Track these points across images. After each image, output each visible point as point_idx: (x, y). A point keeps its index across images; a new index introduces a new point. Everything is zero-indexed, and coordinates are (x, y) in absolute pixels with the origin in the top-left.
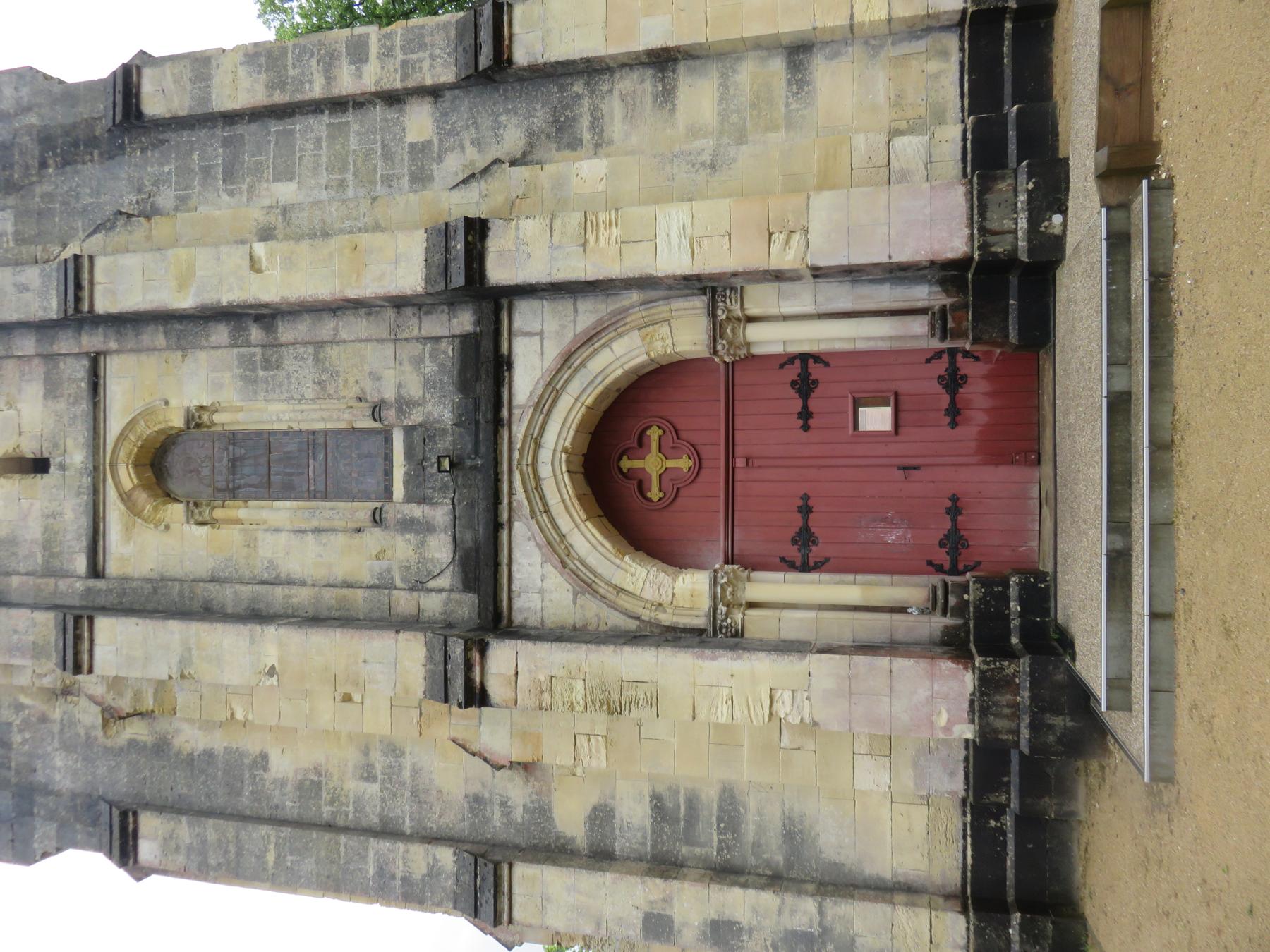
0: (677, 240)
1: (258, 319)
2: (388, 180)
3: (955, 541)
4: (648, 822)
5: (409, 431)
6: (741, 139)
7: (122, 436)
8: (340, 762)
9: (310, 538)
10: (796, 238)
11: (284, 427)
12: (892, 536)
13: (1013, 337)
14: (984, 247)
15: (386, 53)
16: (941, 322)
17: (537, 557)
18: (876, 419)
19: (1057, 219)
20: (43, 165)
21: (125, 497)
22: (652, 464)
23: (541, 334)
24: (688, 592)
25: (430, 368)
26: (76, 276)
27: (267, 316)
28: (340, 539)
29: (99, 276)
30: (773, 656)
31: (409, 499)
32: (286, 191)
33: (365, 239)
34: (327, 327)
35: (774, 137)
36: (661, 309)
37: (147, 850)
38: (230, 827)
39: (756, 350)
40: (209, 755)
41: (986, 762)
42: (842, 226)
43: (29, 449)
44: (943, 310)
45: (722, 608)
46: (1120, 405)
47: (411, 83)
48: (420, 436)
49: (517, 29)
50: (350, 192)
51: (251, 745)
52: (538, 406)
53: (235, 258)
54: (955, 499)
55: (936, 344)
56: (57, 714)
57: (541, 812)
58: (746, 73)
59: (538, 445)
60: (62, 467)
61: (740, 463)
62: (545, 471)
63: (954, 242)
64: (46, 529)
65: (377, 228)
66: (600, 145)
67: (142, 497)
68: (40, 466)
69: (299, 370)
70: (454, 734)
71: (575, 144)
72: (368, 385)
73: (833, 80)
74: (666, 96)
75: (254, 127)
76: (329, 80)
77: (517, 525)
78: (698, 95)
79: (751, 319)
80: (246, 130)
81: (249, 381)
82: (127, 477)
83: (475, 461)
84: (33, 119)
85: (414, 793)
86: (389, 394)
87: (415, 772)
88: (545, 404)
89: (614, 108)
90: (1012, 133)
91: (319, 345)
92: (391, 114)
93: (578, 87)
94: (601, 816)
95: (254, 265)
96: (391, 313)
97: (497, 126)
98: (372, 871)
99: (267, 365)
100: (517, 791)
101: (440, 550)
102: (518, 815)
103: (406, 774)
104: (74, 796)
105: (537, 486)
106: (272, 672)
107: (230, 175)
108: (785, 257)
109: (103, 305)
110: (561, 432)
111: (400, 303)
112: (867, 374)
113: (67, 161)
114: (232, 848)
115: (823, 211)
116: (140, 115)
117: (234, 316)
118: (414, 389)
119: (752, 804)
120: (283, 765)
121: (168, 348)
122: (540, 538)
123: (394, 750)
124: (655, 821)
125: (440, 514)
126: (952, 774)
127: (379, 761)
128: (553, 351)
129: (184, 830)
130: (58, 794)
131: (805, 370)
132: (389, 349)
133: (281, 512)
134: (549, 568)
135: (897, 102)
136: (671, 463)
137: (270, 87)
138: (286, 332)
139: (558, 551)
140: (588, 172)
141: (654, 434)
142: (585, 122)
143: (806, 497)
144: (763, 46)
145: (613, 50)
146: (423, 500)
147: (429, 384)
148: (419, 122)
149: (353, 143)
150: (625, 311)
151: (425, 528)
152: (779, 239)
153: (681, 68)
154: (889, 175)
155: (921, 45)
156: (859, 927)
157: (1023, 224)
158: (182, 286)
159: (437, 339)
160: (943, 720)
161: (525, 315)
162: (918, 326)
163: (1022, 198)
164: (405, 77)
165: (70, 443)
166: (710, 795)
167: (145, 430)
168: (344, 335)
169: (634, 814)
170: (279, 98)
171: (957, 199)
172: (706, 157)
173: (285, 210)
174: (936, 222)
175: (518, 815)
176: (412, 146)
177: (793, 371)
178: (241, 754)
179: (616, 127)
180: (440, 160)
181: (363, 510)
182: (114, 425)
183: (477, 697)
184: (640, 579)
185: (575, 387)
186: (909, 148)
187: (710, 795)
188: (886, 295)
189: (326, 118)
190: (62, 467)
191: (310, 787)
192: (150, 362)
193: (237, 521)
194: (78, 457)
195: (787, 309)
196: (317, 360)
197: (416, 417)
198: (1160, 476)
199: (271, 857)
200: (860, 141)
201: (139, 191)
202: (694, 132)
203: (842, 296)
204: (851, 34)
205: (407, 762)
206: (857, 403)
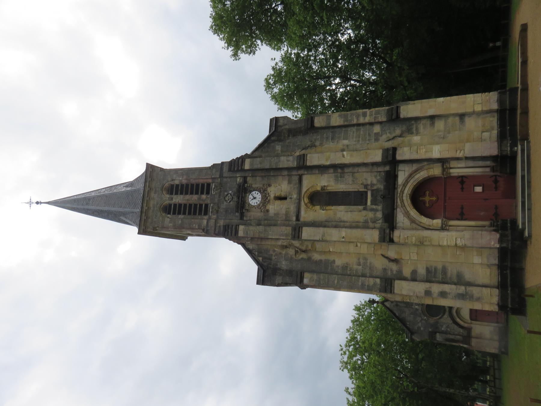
0: (436, 152)
1: (340, 167)
2: (369, 140)
3: (496, 215)
4: (425, 274)
5: (372, 191)
6: (449, 133)
7: (306, 192)
8: (352, 261)
9: (349, 213)
10: (462, 152)
11: (342, 190)
12: (482, 213)
13: (508, 171)
14: (501, 153)
15: (371, 115)
16: (493, 169)
17: (402, 216)
18: (478, 189)
19: (516, 148)
20: (289, 136)
21: (306, 204)
22: (427, 199)
23: (404, 171)
24: (437, 222)
25: (378, 178)
26: (302, 158)
27: (343, 166)
28: (356, 213)
29: (308, 158)
30: (438, 284)
31: (372, 204)
32: (346, 142)
33: (369, 151)
34: (356, 169)
35: (456, 132)
36: (432, 166)
37: (306, 281)
38: (326, 275)
39: (452, 175)
40: (321, 261)
41: (503, 253)
42: (469, 150)
43: (283, 195)
44: (493, 167)
45: (444, 226)
46: (523, 177)
47: (376, 121)
48: (375, 193)
49: (401, 111)
50: (361, 142)
51: (331, 258)
52: (404, 185)
53: (339, 154)
54: (496, 206)
55: (492, 174)
56: (284, 253)
57: (400, 271)
58: (450, 120)
59: (403, 193)
60: (291, 198)
61: (447, 198)
62: (404, 198)
63: (494, 152)
64: (286, 211)
65: (368, 149)
66: (418, 133)
67: (309, 205)
68: (285, 198)
69: (349, 178)
70: (383, 253)
71: (412, 133)
72: (364, 181)
73: (470, 122)
74: (433, 124)
75: (339, 129)
76: (358, 120)
77: (398, 209)
78: (440, 125)
79: (451, 168)
80: (338, 130)
81: (337, 180)
82: (306, 200)
83: (388, 196)
84: (287, 127)
85: (370, 268)
86: (369, 183)
87: (370, 263)
88: (405, 185)
89: (421, 127)
90: (508, 132)
91: (353, 173)
92: (371, 127)
93: (413, 122)
94: (414, 272)
95: (343, 156)
96: (371, 167)
97: (394, 130)
98: (360, 284)
99: (341, 177)
100: (394, 267)
101: (379, 215)
102: (395, 272)
103: (368, 264)
104: (287, 270)
105: (402, 201)
106: (343, 238)
107: (333, 139)
108: (460, 155)
109: (308, 164)
110: (408, 191)
111: (374, 164)
112: (475, 180)
113: (294, 136)
114: (327, 280)
115: (468, 146)
116: (314, 126)
117: (334, 167)
118: (375, 182)
119: (449, 269)
120: (339, 262)
121: (319, 173)
122: (403, 212)
123: (365, 259)
124: (427, 273)
125: (380, 208)
126: (495, 260)
127: (362, 261)
128: (407, 174)
129: (315, 276)
130: (283, 270)
131: (462, 179)
132: (369, 174)
133: (342, 208)
134: (405, 218)
135: (483, 126)
136: (431, 199)
137: (344, 121)
138: (346, 170)
139: (407, 214)
140: (416, 139)
141: (427, 193)
142: (414, 129)
143: (462, 206)
144: (455, 115)
145: (422, 115)
146: (376, 205)
147: (378, 181)
148: (377, 129)
149: (362, 132)
150: (424, 166)
151: (376, 210)
152: (458, 151)
153: (436, 119)
154: (481, 140)
155: (489, 115)
156: (474, 292)
157: (509, 149)
158: (327, 160)
159: (380, 172)
160: (493, 243)
161: (401, 167)
162: (488, 170)
163: (509, 144)
164: (375, 120)
165: (293, 193)
166: (440, 267)
167: (311, 190)
168: (360, 171)
169: (422, 271)
170: (346, 123)
171: (496, 144)
172: (442, 136)
173: (347, 146)
174: (490, 148)
175: (395, 272)
176: (375, 133)
177: (460, 179)
178: (328, 260)
179: (421, 130)
180: (381, 136)
181: (361, 207)
182: (304, 190)
183: (391, 241)
184: (425, 220)
185: (412, 181)
186: (486, 135)
187: (440, 267)
188: (481, 163)
189: (356, 128)
190: (291, 198)
191: (345, 267)
192: (313, 177)
193: (331, 210)
194: (295, 196)
195: (459, 166)
196: (353, 176)
197: (375, 188)
198: (529, 187)
199: (336, 282)
200: (475, 133)
201: (311, 141)
202: (439, 131)
203: (471, 163)
204: (474, 113)
205: (369, 261)
206: (474, 186)
